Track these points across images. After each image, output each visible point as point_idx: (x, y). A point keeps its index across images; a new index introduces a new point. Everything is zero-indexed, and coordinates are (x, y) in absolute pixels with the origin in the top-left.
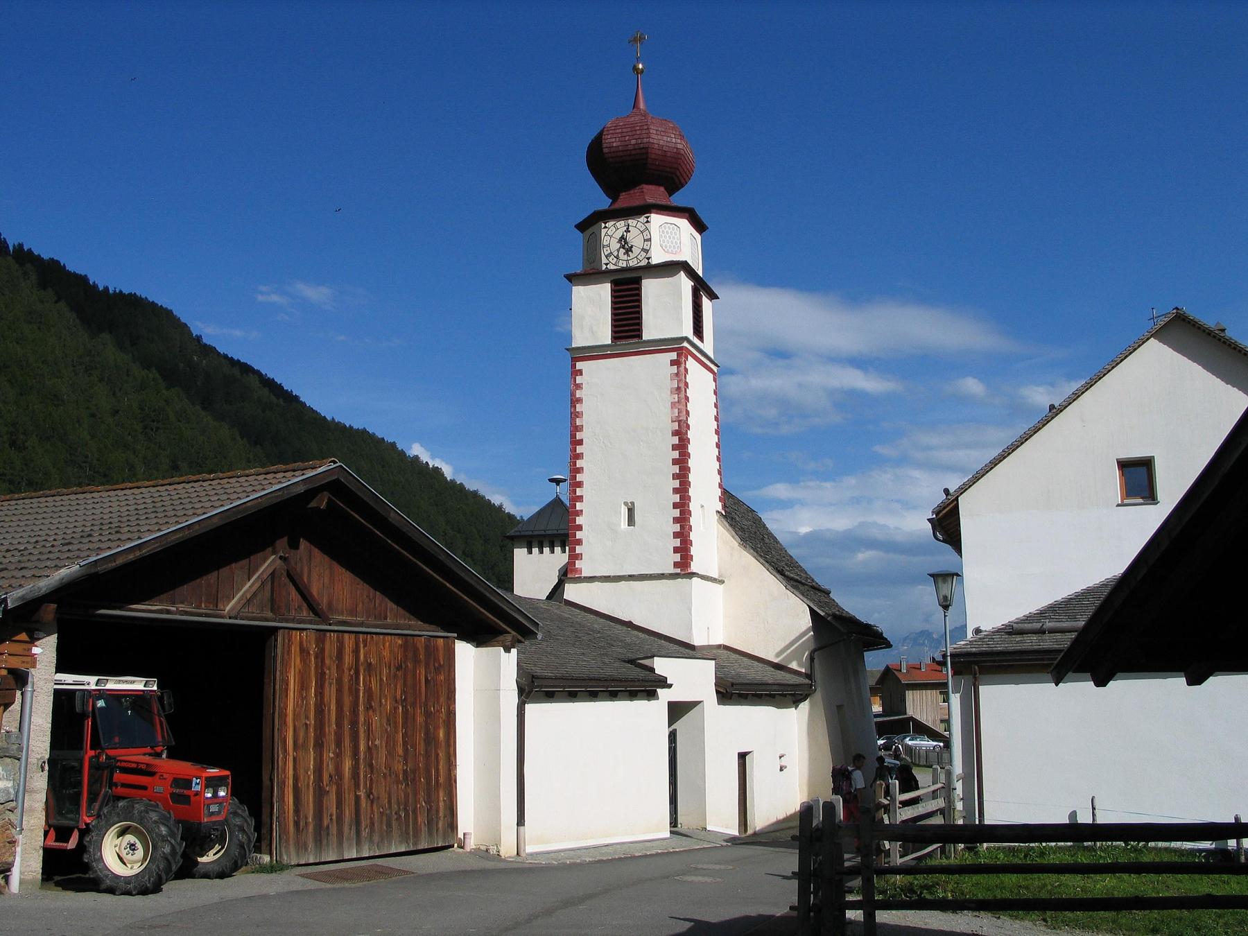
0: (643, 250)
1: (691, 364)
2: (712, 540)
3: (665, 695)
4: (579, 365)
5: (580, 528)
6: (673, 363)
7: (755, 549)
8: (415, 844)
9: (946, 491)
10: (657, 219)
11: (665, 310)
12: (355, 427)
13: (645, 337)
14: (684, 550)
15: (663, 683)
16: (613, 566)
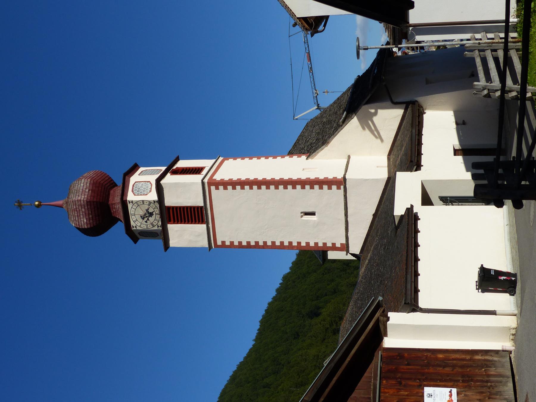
0: (149, 205)
1: (218, 177)
2: (324, 163)
3: (419, 209)
4: (219, 243)
5: (316, 244)
6: (217, 188)
7: (329, 137)
8: (508, 377)
9: (295, 25)
10: (130, 197)
11: (183, 191)
12: (258, 327)
13: (202, 204)
14: (329, 183)
15: (410, 210)
16: (341, 230)
